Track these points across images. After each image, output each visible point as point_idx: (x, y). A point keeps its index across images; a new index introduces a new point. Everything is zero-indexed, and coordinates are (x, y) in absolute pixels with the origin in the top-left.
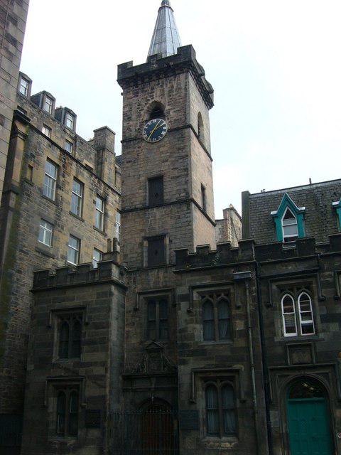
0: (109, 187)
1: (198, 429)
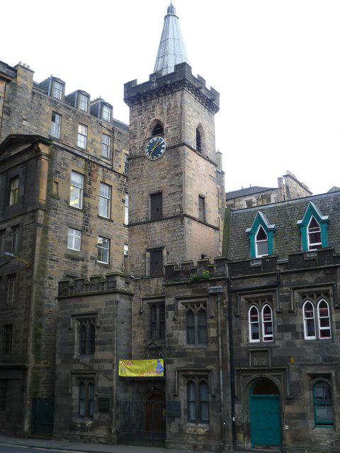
1: (180, 417)
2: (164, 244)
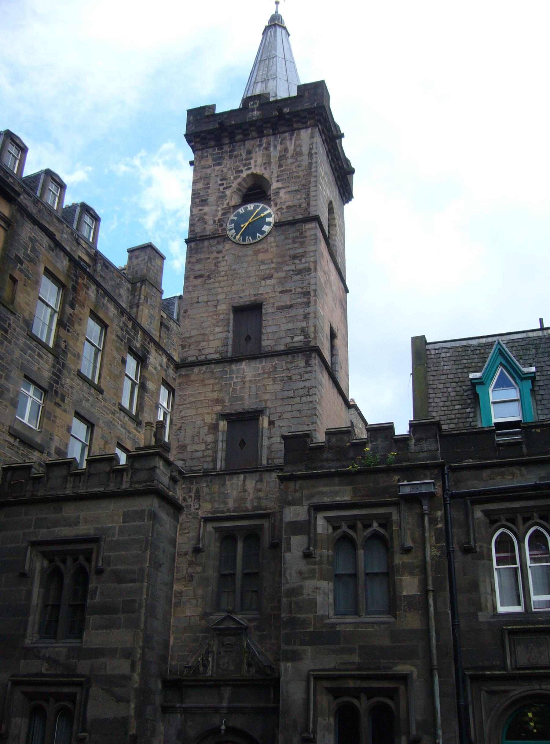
0: (152, 340)
2: (263, 405)
